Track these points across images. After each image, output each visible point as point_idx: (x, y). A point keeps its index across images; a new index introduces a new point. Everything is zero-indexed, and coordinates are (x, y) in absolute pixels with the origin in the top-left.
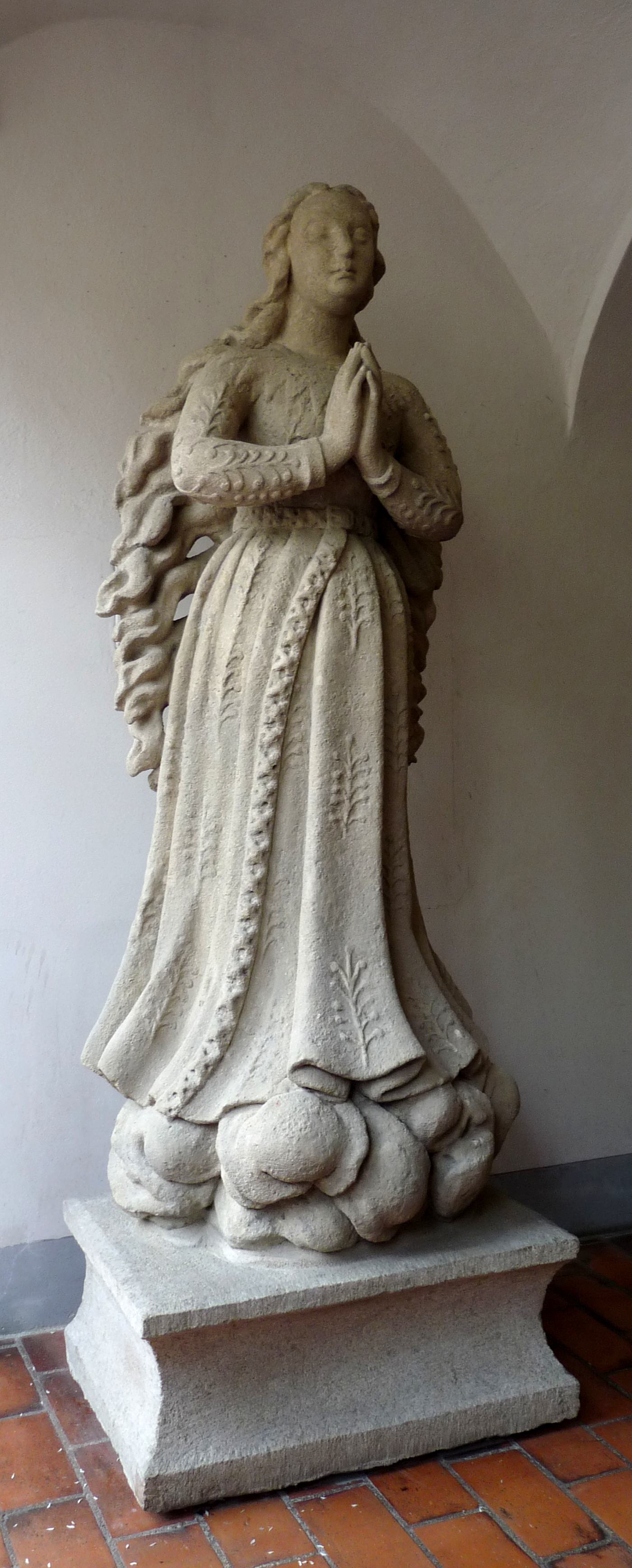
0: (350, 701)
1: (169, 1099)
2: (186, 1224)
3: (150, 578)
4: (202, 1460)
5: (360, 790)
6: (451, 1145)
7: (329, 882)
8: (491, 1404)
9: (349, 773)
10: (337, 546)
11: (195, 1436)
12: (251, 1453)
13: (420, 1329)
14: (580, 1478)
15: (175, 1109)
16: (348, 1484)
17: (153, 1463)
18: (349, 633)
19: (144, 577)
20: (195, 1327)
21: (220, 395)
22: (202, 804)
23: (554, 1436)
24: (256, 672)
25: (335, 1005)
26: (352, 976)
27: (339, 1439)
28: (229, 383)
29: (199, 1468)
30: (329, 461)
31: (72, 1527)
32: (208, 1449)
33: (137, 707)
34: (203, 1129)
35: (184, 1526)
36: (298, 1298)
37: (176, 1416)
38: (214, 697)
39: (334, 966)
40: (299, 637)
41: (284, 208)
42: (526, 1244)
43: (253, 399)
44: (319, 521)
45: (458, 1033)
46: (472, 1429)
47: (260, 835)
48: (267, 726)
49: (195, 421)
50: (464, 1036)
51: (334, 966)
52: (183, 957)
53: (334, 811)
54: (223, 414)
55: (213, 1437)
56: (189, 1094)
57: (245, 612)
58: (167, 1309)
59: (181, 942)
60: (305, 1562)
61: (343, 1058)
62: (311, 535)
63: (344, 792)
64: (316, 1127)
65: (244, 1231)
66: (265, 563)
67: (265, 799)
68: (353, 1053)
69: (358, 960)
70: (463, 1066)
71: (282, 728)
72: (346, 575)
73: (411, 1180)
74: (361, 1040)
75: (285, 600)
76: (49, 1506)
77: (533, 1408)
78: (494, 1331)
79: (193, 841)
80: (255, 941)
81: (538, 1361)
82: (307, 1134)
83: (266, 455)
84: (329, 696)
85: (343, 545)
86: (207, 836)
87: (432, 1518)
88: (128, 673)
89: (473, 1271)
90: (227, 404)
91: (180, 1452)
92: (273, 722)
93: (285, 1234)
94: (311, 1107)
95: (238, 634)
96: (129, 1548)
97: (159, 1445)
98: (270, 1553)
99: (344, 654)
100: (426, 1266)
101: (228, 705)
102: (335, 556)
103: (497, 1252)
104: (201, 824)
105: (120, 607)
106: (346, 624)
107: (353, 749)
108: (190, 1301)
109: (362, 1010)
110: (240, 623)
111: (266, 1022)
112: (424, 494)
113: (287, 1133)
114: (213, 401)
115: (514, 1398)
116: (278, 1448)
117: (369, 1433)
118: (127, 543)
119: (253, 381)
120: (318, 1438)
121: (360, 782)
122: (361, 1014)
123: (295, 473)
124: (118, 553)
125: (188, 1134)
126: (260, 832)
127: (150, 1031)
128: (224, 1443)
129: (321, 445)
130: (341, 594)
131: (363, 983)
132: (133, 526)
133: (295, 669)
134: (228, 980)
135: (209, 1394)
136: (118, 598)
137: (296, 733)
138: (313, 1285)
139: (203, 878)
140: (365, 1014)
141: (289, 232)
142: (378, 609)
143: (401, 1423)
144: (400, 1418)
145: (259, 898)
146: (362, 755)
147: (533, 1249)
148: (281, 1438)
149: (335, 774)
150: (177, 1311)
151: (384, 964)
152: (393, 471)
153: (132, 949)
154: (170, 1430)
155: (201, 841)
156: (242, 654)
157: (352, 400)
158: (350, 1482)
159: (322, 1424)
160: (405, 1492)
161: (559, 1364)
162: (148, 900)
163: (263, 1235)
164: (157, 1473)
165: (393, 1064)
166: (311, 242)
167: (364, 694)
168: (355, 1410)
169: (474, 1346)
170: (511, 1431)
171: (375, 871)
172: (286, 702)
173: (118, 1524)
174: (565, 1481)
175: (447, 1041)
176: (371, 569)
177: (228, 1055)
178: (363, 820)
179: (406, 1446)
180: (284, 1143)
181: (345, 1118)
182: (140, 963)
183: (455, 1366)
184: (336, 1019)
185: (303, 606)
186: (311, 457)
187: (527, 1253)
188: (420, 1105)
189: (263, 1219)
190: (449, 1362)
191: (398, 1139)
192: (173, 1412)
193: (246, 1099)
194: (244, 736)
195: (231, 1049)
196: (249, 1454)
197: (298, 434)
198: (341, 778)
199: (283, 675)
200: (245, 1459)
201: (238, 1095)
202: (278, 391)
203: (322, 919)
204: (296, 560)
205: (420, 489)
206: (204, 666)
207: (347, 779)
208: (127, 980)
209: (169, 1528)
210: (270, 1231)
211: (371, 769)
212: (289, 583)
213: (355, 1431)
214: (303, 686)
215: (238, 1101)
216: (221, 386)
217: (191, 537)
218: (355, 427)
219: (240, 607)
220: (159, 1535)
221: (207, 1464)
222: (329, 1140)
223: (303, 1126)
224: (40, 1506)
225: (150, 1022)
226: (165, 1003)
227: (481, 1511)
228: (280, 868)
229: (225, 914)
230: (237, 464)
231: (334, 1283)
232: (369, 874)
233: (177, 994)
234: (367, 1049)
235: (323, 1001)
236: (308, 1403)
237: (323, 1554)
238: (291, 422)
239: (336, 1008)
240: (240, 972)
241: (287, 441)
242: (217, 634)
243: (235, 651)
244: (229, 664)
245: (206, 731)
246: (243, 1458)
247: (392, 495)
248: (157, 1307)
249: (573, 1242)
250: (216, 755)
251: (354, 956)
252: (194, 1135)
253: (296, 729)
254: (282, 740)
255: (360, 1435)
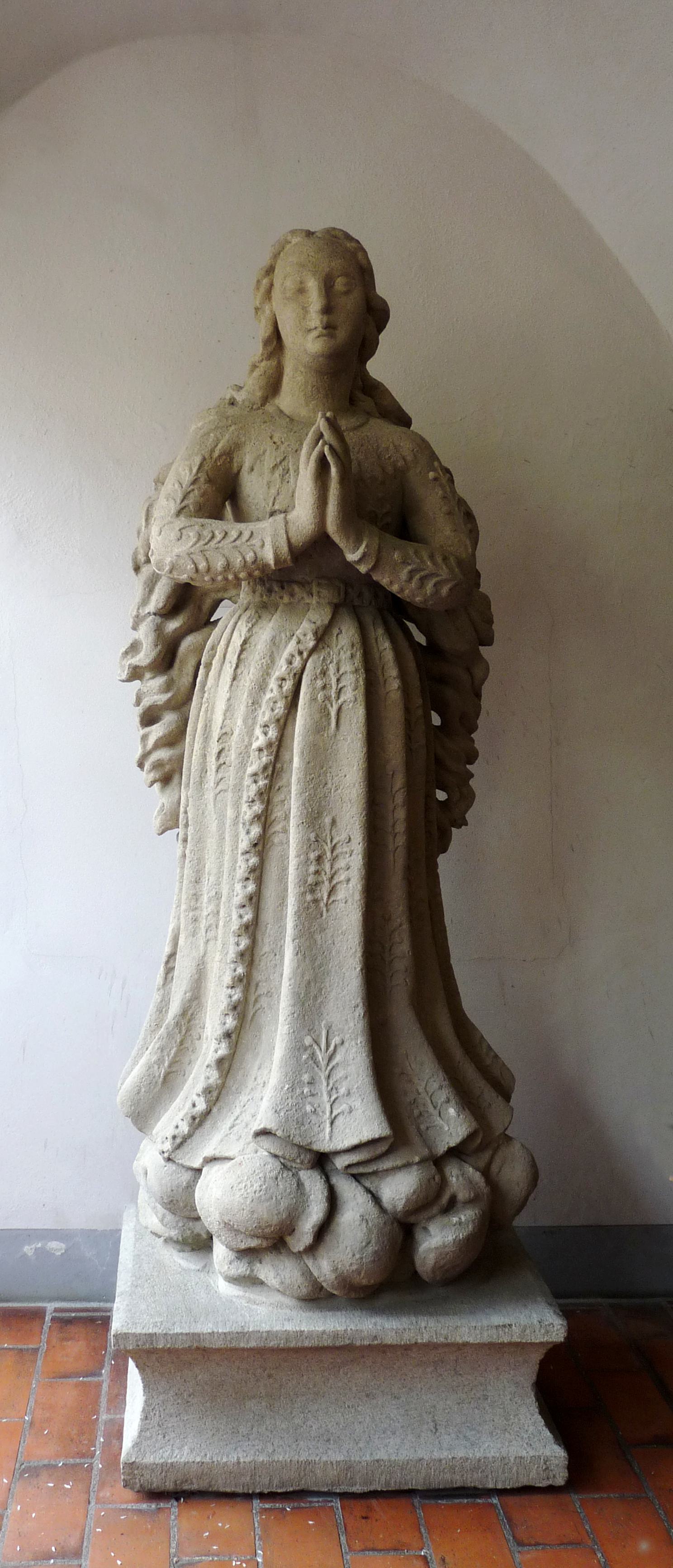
0: (330, 782)
1: (163, 1142)
2: (193, 1250)
3: (159, 647)
4: (176, 1457)
5: (341, 871)
6: (430, 1219)
7: (307, 959)
8: (467, 1459)
9: (329, 854)
10: (319, 623)
11: (173, 1435)
12: (222, 1459)
13: (400, 1379)
14: (537, 1544)
15: (167, 1152)
16: (318, 1502)
17: (131, 1451)
18: (329, 714)
19: (153, 647)
20: (161, 1347)
21: (195, 470)
22: (204, 871)
23: (537, 1498)
24: (239, 751)
25: (306, 1078)
26: (326, 1052)
27: (308, 1463)
28: (207, 457)
29: (172, 1464)
30: (293, 541)
31: (68, 1487)
32: (183, 1448)
33: (154, 771)
34: (193, 1172)
35: (159, 1506)
36: (262, 1337)
37: (157, 1415)
38: (211, 769)
39: (308, 1041)
40: (277, 717)
41: (265, 261)
42: (507, 1321)
43: (235, 470)
44: (305, 595)
45: (452, 1111)
46: (448, 1476)
47: (244, 909)
48: (248, 804)
49: (167, 500)
50: (459, 1115)
51: (308, 1041)
52: (190, 1012)
53: (312, 891)
54: (196, 492)
55: (189, 1439)
56: (178, 1141)
57: (233, 688)
58: (135, 1328)
59: (187, 998)
60: (239, 1563)
61: (306, 1130)
62: (295, 610)
63: (323, 873)
64: (271, 1191)
65: (226, 1267)
66: (252, 640)
67: (246, 875)
68: (317, 1125)
69: (335, 1036)
70: (453, 1144)
71: (262, 807)
72: (329, 653)
73: (370, 1249)
74: (328, 1114)
75: (264, 680)
76: (60, 1465)
77: (515, 1469)
78: (482, 1393)
79: (198, 905)
80: (239, 1009)
81: (526, 1428)
82: (261, 1196)
83: (233, 536)
84: (306, 778)
85: (326, 622)
86: (209, 901)
87: (373, 1550)
88: (144, 738)
89: (446, 1338)
90: (202, 480)
91: (157, 1445)
92: (253, 801)
93: (262, 1277)
94: (270, 1172)
95: (227, 711)
96: (103, 1515)
97: (139, 1436)
98: (215, 1547)
99: (323, 735)
100: (395, 1327)
101: (221, 779)
102: (315, 633)
103: (485, 1323)
104: (205, 889)
105: (136, 674)
106: (326, 705)
107: (333, 832)
108: (159, 1324)
109: (334, 1085)
110: (229, 700)
111: (251, 1084)
112: (410, 568)
113: (242, 1193)
114: (187, 479)
115: (493, 1457)
116: (248, 1459)
117: (338, 1463)
118: (140, 611)
119: (233, 452)
120: (287, 1458)
121: (341, 863)
122: (332, 1089)
123: (259, 555)
124: (134, 621)
125: (180, 1175)
126: (244, 906)
127: (159, 1076)
128: (199, 1446)
129: (286, 523)
130: (321, 673)
131: (338, 1058)
132: (144, 595)
133: (274, 749)
134: (215, 1041)
135: (188, 1402)
136: (132, 666)
137: (279, 811)
138: (277, 1328)
139: (208, 941)
140: (336, 1089)
141: (272, 285)
142: (362, 689)
143: (372, 1459)
144: (372, 1454)
145: (244, 968)
146: (343, 837)
147: (514, 1327)
148: (252, 1452)
149: (312, 856)
150: (144, 1331)
151: (361, 1042)
152: (367, 546)
153: (157, 997)
154: (151, 1426)
155: (204, 905)
156: (232, 730)
157: (310, 478)
158: (321, 1499)
159: (294, 1446)
160: (364, 1521)
161: (549, 1434)
162: (169, 953)
163: (243, 1274)
164: (133, 1459)
165: (355, 1141)
166: (288, 299)
167: (345, 776)
168: (328, 1440)
169: (459, 1404)
170: (491, 1486)
171: (356, 951)
172: (266, 782)
173: (106, 1493)
174: (520, 1544)
175: (438, 1118)
176: (358, 646)
177: (215, 1110)
178: (344, 901)
179: (377, 1480)
180: (239, 1202)
181: (307, 1184)
182: (164, 1010)
183: (436, 1418)
184: (305, 1092)
185: (281, 686)
186: (275, 536)
187: (507, 1330)
188: (389, 1179)
189: (243, 1260)
190: (430, 1413)
191: (362, 1210)
192: (154, 1412)
193: (220, 1154)
194: (230, 813)
195: (218, 1104)
196: (219, 1459)
197: (277, 507)
198: (319, 859)
199: (262, 755)
200: (215, 1463)
201: (215, 1149)
202: (258, 461)
203: (298, 994)
204: (277, 638)
205: (405, 563)
206: (202, 739)
207: (326, 860)
208: (153, 1024)
209: (144, 1506)
210: (248, 1272)
211: (352, 851)
212: (269, 662)
213: (324, 1458)
214: (285, 766)
215: (214, 1155)
216: (198, 460)
217: (208, 602)
218: (316, 505)
219: (229, 683)
220: (133, 1510)
221: (179, 1460)
222: (283, 1205)
223: (258, 1188)
224: (54, 1463)
225: (159, 1068)
226: (173, 1052)
227: (423, 1554)
228: (266, 940)
229: (217, 979)
230: (200, 546)
231: (298, 1329)
232: (350, 953)
233: (186, 1045)
234: (332, 1123)
235: (293, 1073)
236: (283, 1426)
237: (260, 1560)
238: (270, 495)
239: (306, 1081)
240: (224, 1035)
241: (268, 516)
242: (213, 707)
243: (225, 726)
244: (219, 739)
245: (205, 802)
246: (213, 1462)
247: (374, 568)
248: (128, 1324)
249: (559, 1327)
250: (213, 827)
251: (330, 1031)
252: (186, 1176)
253: (279, 807)
254: (263, 818)
255: (329, 1462)
